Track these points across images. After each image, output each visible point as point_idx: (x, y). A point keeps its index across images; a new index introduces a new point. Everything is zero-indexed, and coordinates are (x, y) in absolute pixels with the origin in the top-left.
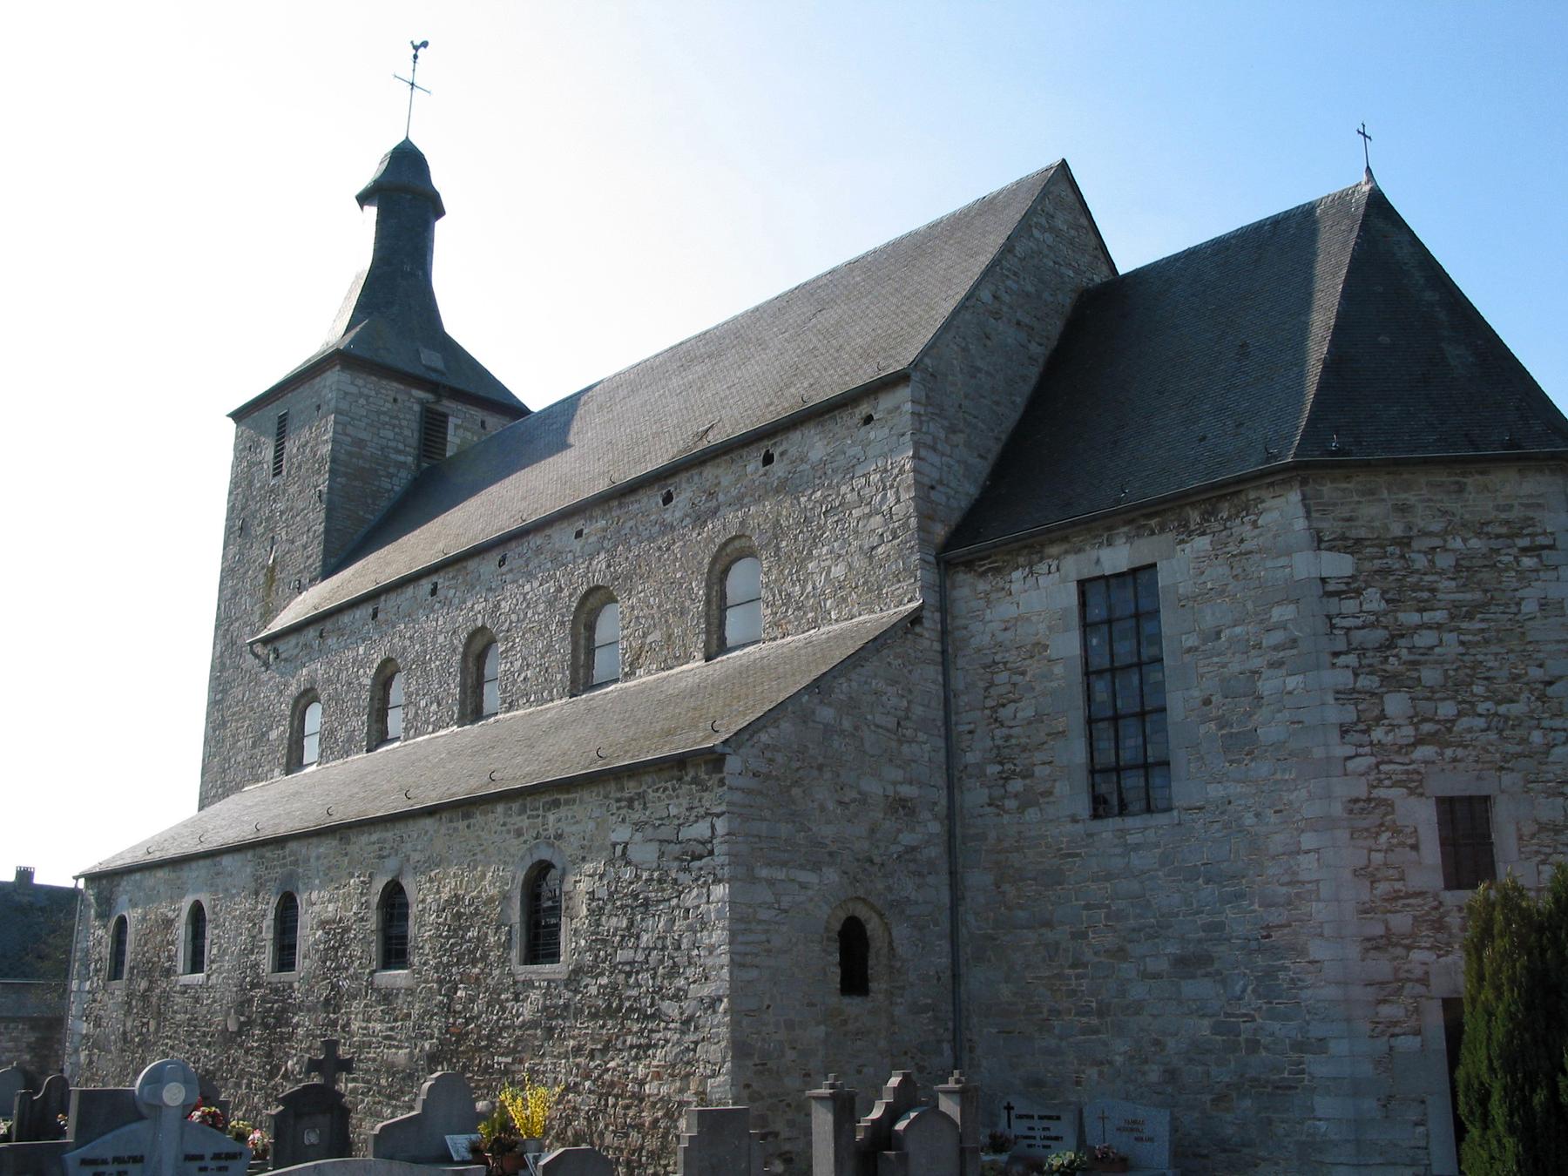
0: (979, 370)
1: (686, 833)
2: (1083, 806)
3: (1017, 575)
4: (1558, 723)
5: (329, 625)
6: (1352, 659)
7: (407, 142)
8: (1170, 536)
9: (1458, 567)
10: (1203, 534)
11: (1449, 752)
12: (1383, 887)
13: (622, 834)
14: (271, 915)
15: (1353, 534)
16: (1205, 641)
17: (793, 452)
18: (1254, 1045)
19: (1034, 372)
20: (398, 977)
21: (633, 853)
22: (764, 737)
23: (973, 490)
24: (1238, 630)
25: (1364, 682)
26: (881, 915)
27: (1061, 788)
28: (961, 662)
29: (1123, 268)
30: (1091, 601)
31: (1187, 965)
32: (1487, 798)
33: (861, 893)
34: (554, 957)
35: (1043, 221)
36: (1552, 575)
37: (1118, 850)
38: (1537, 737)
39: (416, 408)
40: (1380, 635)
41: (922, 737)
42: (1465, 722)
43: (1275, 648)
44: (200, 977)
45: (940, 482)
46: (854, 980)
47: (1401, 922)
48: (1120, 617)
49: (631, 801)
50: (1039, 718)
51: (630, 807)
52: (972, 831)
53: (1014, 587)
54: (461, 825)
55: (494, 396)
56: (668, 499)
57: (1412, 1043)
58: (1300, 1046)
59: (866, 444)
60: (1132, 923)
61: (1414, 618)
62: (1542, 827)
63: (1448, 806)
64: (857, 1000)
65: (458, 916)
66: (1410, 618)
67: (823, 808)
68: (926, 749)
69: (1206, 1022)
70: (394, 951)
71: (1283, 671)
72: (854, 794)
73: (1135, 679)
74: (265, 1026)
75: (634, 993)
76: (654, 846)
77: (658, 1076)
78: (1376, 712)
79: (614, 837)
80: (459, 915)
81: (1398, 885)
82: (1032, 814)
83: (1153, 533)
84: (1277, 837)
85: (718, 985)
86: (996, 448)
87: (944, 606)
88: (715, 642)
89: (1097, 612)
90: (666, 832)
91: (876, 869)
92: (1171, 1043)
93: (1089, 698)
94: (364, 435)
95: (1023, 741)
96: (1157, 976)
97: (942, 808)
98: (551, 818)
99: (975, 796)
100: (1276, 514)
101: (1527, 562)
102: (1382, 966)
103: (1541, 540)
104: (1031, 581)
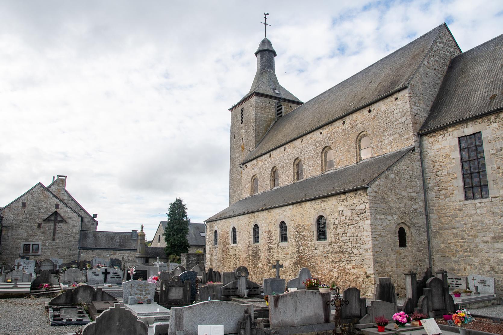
0: (425, 83)
2: (462, 197)
3: (440, 137)
5: (259, 159)
7: (266, 38)
10: (495, 122)
13: (341, 208)
14: (252, 230)
17: (377, 109)
19: (440, 82)
22: (377, 183)
23: (426, 115)
26: (409, 227)
27: (456, 192)
28: (426, 160)
29: (463, 52)
30: (462, 142)
33: (403, 221)
34: (325, 238)
35: (440, 40)
44: (235, 245)
45: (417, 114)
46: (403, 243)
49: (343, 200)
50: (449, 174)
51: (343, 201)
52: (431, 204)
53: (440, 140)
54: (299, 207)
55: (294, 100)
56: (344, 123)
60: (479, 228)
64: (403, 248)
67: (392, 200)
68: (419, 183)
70: (284, 238)
72: (400, 196)
73: (476, 163)
74: (253, 256)
77: (353, 268)
79: (339, 209)
80: (300, 229)
82: (448, 199)
83: (480, 123)
85: (369, 245)
86: (431, 104)
87: (421, 146)
88: (359, 158)
89: (463, 145)
91: (406, 215)
92: (492, 260)
93: (463, 169)
95: (444, 180)
96: (486, 242)
97: (423, 198)
98: (322, 205)
99: (431, 195)
104: (444, 138)
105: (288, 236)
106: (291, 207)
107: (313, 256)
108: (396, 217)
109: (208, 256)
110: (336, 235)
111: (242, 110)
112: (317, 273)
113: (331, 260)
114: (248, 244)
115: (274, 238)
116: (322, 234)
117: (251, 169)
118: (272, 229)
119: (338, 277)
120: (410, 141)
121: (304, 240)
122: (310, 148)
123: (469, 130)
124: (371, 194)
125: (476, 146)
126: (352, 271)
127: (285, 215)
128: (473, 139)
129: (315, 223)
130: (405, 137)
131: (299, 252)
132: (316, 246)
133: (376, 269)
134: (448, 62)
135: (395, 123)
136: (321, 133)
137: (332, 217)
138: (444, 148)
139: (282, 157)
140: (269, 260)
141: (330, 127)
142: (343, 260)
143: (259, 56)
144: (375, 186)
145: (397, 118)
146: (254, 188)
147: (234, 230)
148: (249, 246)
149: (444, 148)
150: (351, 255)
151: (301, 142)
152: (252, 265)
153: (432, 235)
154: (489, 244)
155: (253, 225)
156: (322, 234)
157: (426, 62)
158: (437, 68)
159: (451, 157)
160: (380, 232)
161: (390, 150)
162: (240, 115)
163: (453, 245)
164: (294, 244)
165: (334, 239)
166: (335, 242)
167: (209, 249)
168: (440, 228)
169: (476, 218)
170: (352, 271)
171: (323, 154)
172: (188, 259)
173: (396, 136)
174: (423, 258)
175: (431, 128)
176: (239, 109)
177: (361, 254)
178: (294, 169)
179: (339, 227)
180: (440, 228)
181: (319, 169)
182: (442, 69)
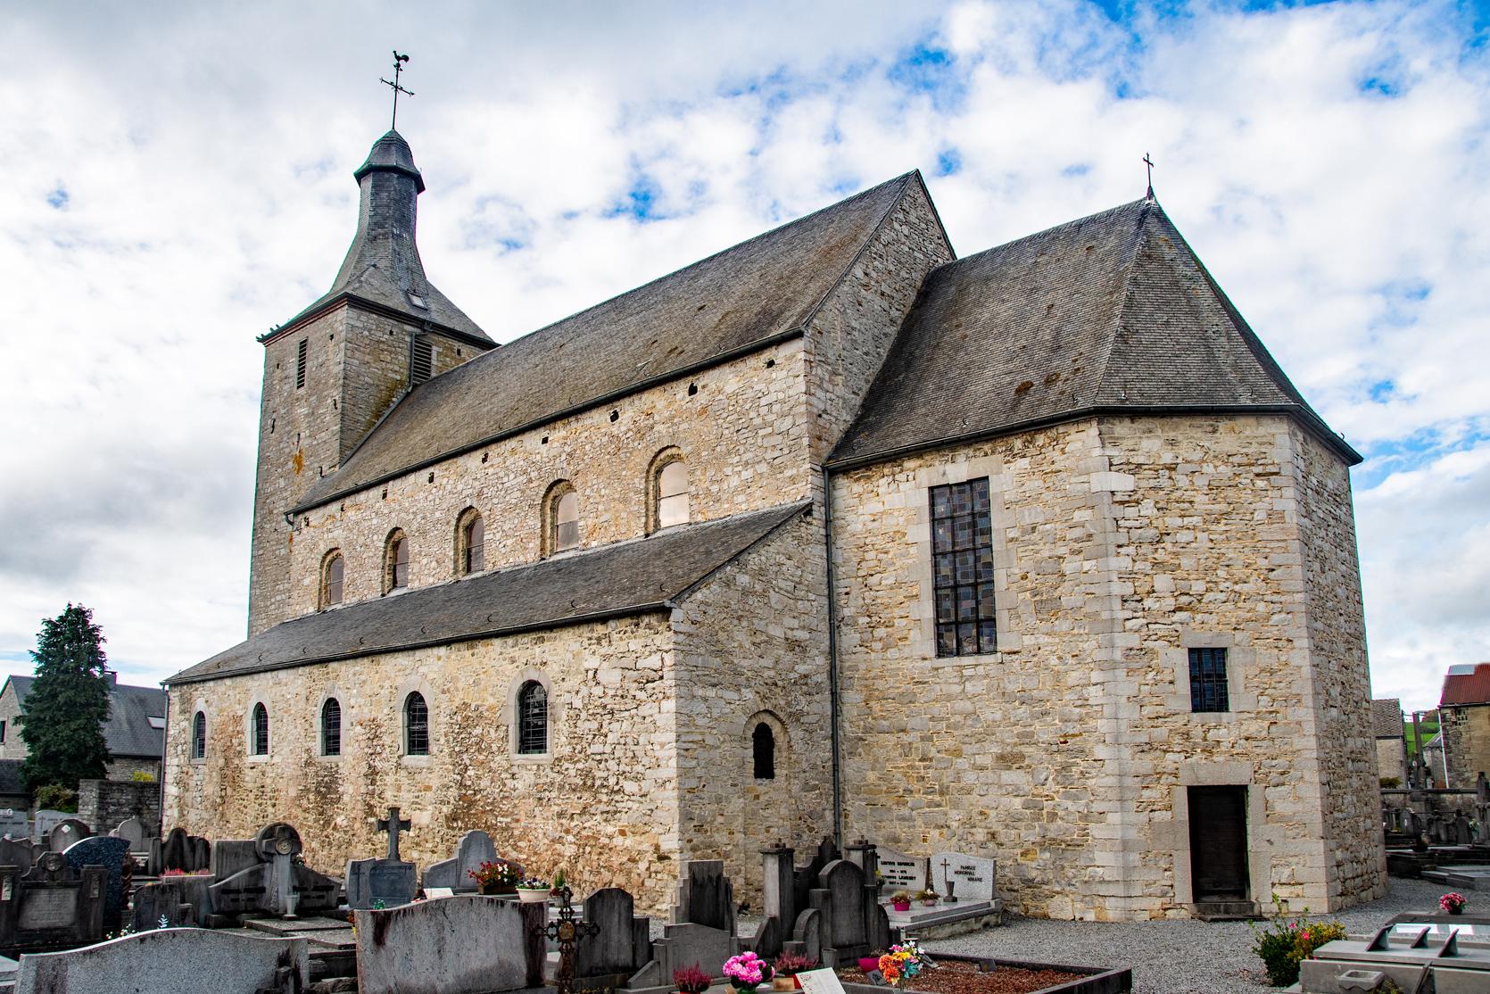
2: (930, 648)
3: (883, 481)
4: (1276, 598)
5: (348, 502)
6: (1131, 550)
13: (592, 662)
15: (1134, 460)
17: (712, 386)
18: (1053, 816)
19: (893, 331)
23: (850, 418)
25: (1139, 566)
26: (783, 723)
28: (839, 543)
29: (960, 256)
33: (769, 706)
34: (541, 748)
35: (901, 216)
38: (1261, 607)
40: (1152, 532)
42: (1209, 596)
43: (1076, 540)
44: (262, 758)
45: (825, 411)
46: (764, 768)
47: (1161, 733)
49: (599, 640)
50: (898, 585)
53: (880, 490)
56: (615, 417)
58: (1085, 817)
60: (967, 731)
61: (1179, 522)
65: (466, 719)
67: (741, 646)
70: (418, 743)
72: (764, 638)
73: (971, 559)
77: (623, 833)
78: (1148, 588)
79: (587, 665)
84: (1074, 674)
86: (866, 387)
87: (829, 504)
88: (651, 523)
90: (627, 662)
92: (992, 813)
93: (936, 571)
96: (982, 769)
98: (537, 650)
99: (849, 638)
100: (1079, 444)
101: (1260, 483)
102: (1146, 763)
104: (893, 486)
105: (431, 737)
106: (442, 651)
108: (748, 694)
109: (171, 790)
110: (574, 737)
112: (515, 847)
113: (556, 809)
115: (387, 740)
116: (532, 736)
117: (323, 530)
118: (382, 714)
119: (577, 857)
120: (800, 487)
121: (480, 750)
122: (511, 481)
123: (959, 469)
124: (682, 628)
125: (973, 515)
126: (618, 840)
127: (425, 675)
129: (513, 702)
130: (788, 473)
131: (461, 785)
132: (515, 769)
134: (918, 277)
135: (761, 432)
136: (545, 441)
137: (565, 685)
138: (890, 513)
139: (425, 503)
140: (371, 807)
141: (574, 425)
142: (592, 810)
144: (694, 606)
145: (771, 418)
146: (330, 588)
147: (260, 711)
148: (307, 764)
149: (890, 513)
150: (617, 797)
151: (484, 460)
152: (316, 821)
153: (844, 747)
155: (321, 699)
158: (888, 291)
159: (909, 539)
161: (744, 507)
162: (294, 360)
164: (448, 760)
165: (567, 750)
167: (176, 770)
168: (868, 730)
170: (618, 840)
171: (549, 503)
172: (102, 798)
173: (763, 468)
174: (819, 809)
175: (859, 455)
176: (294, 339)
178: (456, 539)
179: (584, 715)
180: (868, 730)
181: (535, 544)
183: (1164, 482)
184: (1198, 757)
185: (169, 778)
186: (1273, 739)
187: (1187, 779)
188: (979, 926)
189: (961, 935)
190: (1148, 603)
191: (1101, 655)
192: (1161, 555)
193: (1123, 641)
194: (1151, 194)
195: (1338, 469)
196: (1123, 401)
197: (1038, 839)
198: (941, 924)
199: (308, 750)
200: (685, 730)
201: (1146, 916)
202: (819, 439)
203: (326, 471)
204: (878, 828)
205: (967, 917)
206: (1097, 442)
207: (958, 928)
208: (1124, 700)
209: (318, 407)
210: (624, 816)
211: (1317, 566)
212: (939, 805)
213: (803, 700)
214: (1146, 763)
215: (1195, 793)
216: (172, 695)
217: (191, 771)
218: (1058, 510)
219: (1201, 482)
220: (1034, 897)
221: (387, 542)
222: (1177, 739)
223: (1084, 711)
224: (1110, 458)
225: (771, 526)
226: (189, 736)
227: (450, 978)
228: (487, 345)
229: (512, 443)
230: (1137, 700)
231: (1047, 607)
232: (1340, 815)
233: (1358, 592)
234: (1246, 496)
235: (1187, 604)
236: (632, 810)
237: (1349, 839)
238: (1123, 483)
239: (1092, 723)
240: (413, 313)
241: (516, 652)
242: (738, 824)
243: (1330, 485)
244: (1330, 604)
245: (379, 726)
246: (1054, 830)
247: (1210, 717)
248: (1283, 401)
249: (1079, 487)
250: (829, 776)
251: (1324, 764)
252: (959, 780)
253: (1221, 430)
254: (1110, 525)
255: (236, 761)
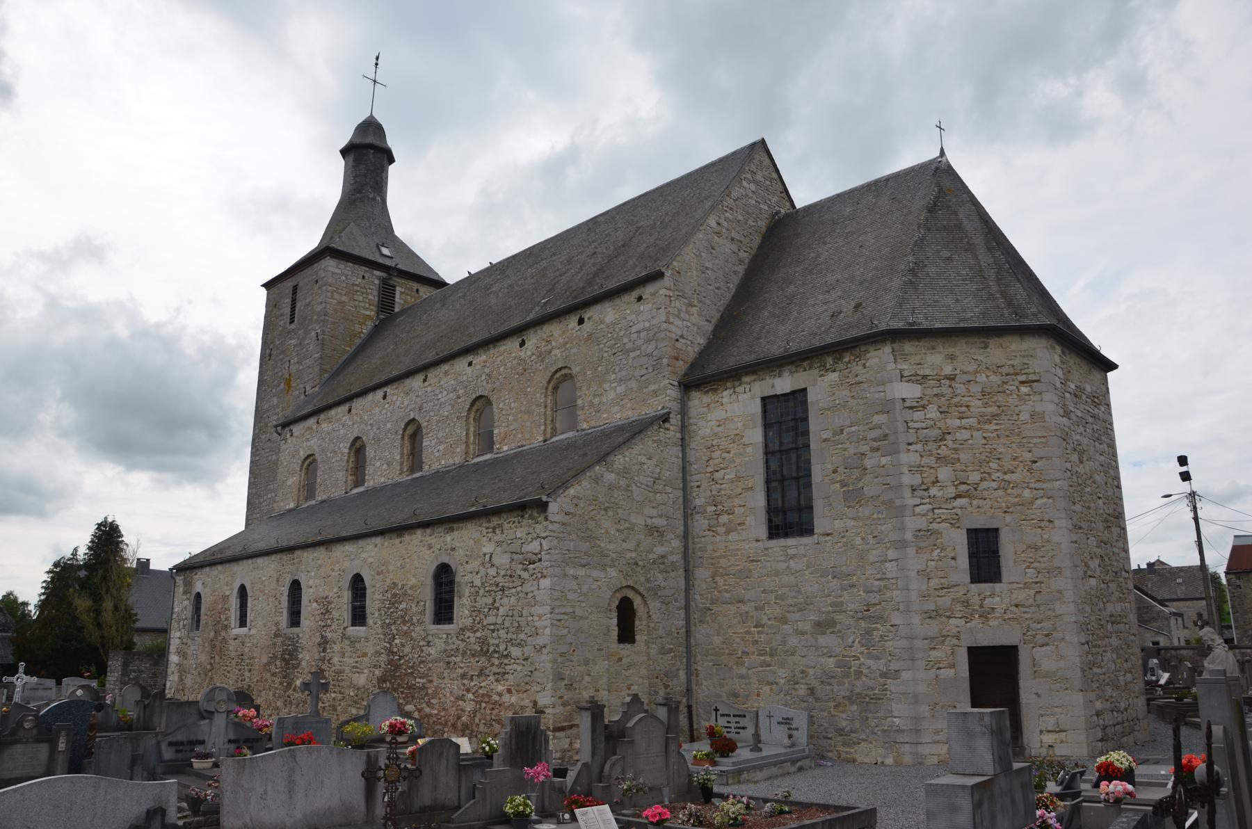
0: (707, 268)
1: (525, 549)
2: (763, 531)
3: (725, 393)
4: (1038, 485)
5: (322, 416)
6: (919, 447)
8: (816, 372)
9: (983, 393)
11: (975, 502)
12: (934, 583)
13: (488, 548)
14: (286, 593)
15: (921, 372)
16: (834, 435)
17: (596, 317)
18: (859, 674)
19: (741, 269)
20: (359, 631)
21: (496, 560)
23: (702, 341)
24: (853, 429)
25: (926, 460)
26: (642, 596)
28: (693, 445)
29: (799, 204)
31: (822, 626)
32: (997, 530)
33: (630, 583)
34: (450, 620)
35: (749, 176)
36: (1038, 397)
37: (783, 558)
39: (377, 282)
41: (669, 489)
42: (984, 485)
43: (874, 440)
44: (244, 630)
45: (682, 336)
46: (626, 634)
47: (945, 601)
48: (786, 422)
49: (494, 529)
50: (738, 478)
53: (725, 400)
54: (397, 541)
56: (522, 344)
57: (951, 672)
58: (885, 675)
59: (639, 313)
60: (790, 601)
61: (957, 422)
62: (1029, 547)
63: (973, 534)
64: (628, 646)
65: (396, 597)
66: (953, 422)
67: (607, 532)
68: (673, 495)
69: (832, 659)
70: (359, 617)
71: (879, 453)
72: (627, 525)
73: (794, 456)
74: (283, 659)
75: (496, 642)
76: (509, 555)
77: (509, 691)
78: (933, 479)
79: (485, 550)
80: (395, 595)
81: (943, 581)
84: (874, 552)
86: (717, 316)
87: (684, 412)
88: (549, 431)
90: (514, 547)
92: (811, 672)
93: (768, 468)
94: (344, 298)
95: (729, 492)
96: (803, 633)
98: (448, 538)
99: (700, 523)
100: (877, 360)
101: (1024, 389)
102: (932, 628)
103: (1032, 377)
104: (734, 397)
105: (368, 611)
106: (378, 540)
107: (422, 662)
108: (613, 573)
109: (174, 658)
110: (475, 611)
111: (295, 289)
112: (429, 704)
113: (460, 671)
114: (274, 628)
115: (335, 614)
116: (444, 612)
117: (303, 440)
118: (332, 592)
119: (475, 712)
120: (665, 397)
121: (404, 622)
122: (443, 396)
123: (783, 384)
124: (557, 518)
125: (795, 420)
126: (506, 698)
127: (365, 560)
128: (791, 404)
129: (429, 581)
130: (652, 388)
131: (390, 652)
132: (430, 638)
133: (559, 694)
134: (763, 224)
135: (632, 355)
136: (470, 364)
137: (468, 567)
138: (734, 416)
139: (378, 415)
141: (492, 351)
142: (487, 672)
143: (351, 158)
144: (567, 500)
145: (639, 342)
146: (309, 489)
147: (243, 591)
148: (276, 635)
149: (734, 416)
150: (506, 661)
151: (425, 381)
152: (281, 683)
153: (695, 616)
154: (808, 636)
156: (444, 612)
157: (712, 222)
158: (737, 237)
159: (745, 440)
160: (573, 607)
161: (618, 416)
162: (288, 301)
163: (738, 640)
164: (380, 630)
166: (472, 629)
167: (177, 641)
168: (714, 601)
169: (787, 579)
170: (506, 698)
171: (473, 415)
172: (125, 665)
173: (633, 384)
174: (674, 669)
175: (711, 369)
176: (289, 284)
177: (526, 659)
178: (402, 445)
179: (481, 592)
180: (714, 601)
181: (460, 449)
182: (748, 240)
183: (945, 389)
184: (976, 622)
185: (173, 648)
186: (1038, 606)
187: (968, 641)
188: (794, 769)
189: (777, 777)
190: (934, 491)
191: (894, 536)
192: (944, 451)
193: (912, 524)
194: (942, 153)
195: (1097, 375)
196: (910, 324)
197: (847, 693)
198: (760, 768)
199: (277, 624)
200: (558, 603)
201: (934, 760)
202: (677, 359)
203: (309, 391)
204: (721, 685)
205: (785, 761)
206: (891, 358)
207: (774, 771)
208: (914, 574)
209: (304, 339)
210: (511, 677)
211: (1075, 457)
212: (769, 666)
213: (660, 577)
214: (932, 628)
215: (974, 652)
216: (178, 579)
217: (189, 642)
218: (860, 415)
219: (975, 389)
220: (845, 744)
221: (350, 449)
222: (959, 607)
223: (882, 583)
224: (901, 371)
225: (634, 431)
226: (188, 613)
227: (298, 814)
228: (439, 284)
229: (445, 367)
230: (924, 574)
231: (853, 496)
232: (1099, 671)
233: (1117, 478)
234: (1013, 400)
235: (967, 492)
236: (517, 671)
237: (1109, 691)
238: (910, 391)
239: (889, 594)
240: (381, 260)
241: (431, 540)
242: (603, 682)
243: (1088, 389)
244: (1088, 489)
245: (330, 603)
246: (859, 685)
247: (986, 587)
248: (1047, 320)
249: (876, 396)
250: (682, 640)
251: (1084, 627)
252: (784, 642)
253: (991, 346)
254: (901, 427)
255: (223, 634)
